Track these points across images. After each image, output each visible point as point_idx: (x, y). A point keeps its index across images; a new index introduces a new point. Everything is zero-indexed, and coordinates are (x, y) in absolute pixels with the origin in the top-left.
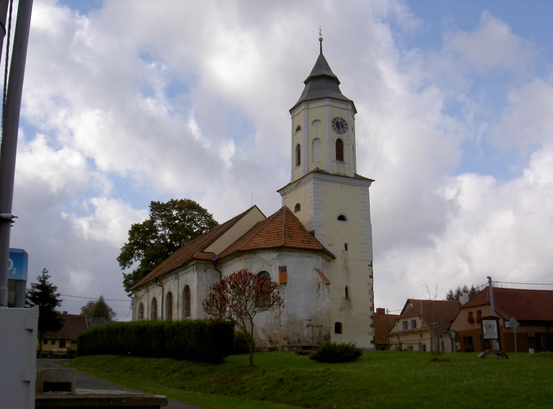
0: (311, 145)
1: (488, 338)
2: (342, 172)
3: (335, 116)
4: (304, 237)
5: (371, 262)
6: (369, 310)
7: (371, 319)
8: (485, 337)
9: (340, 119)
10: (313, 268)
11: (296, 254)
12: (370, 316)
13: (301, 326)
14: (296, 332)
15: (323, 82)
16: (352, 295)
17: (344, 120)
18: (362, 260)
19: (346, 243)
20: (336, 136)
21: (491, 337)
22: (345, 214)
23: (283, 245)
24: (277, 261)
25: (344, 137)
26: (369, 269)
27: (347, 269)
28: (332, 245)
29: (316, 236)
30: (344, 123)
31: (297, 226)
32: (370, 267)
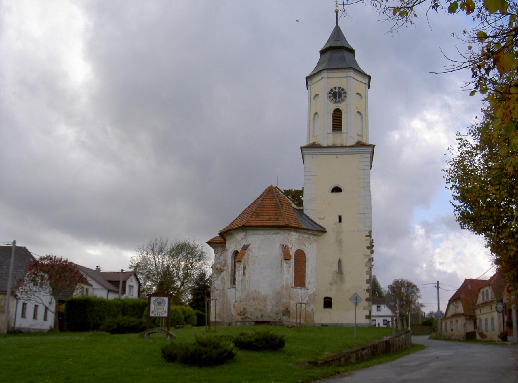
0: (312, 120)
1: (156, 315)
2: (338, 143)
3: (332, 87)
4: (274, 214)
5: (370, 232)
6: (365, 282)
7: (367, 293)
8: (151, 315)
9: (338, 88)
10: (279, 245)
11: (262, 232)
12: (366, 290)
13: (265, 301)
14: (259, 308)
15: (337, 54)
16: (346, 268)
17: (342, 88)
18: (358, 231)
19: (340, 214)
20: (333, 107)
21: (159, 314)
22: (341, 186)
23: (288, 225)
24: (244, 240)
25: (341, 106)
26: (367, 240)
27: (340, 242)
28: (323, 218)
29: (305, 211)
30: (342, 92)
31: (273, 204)
32: (369, 238)
